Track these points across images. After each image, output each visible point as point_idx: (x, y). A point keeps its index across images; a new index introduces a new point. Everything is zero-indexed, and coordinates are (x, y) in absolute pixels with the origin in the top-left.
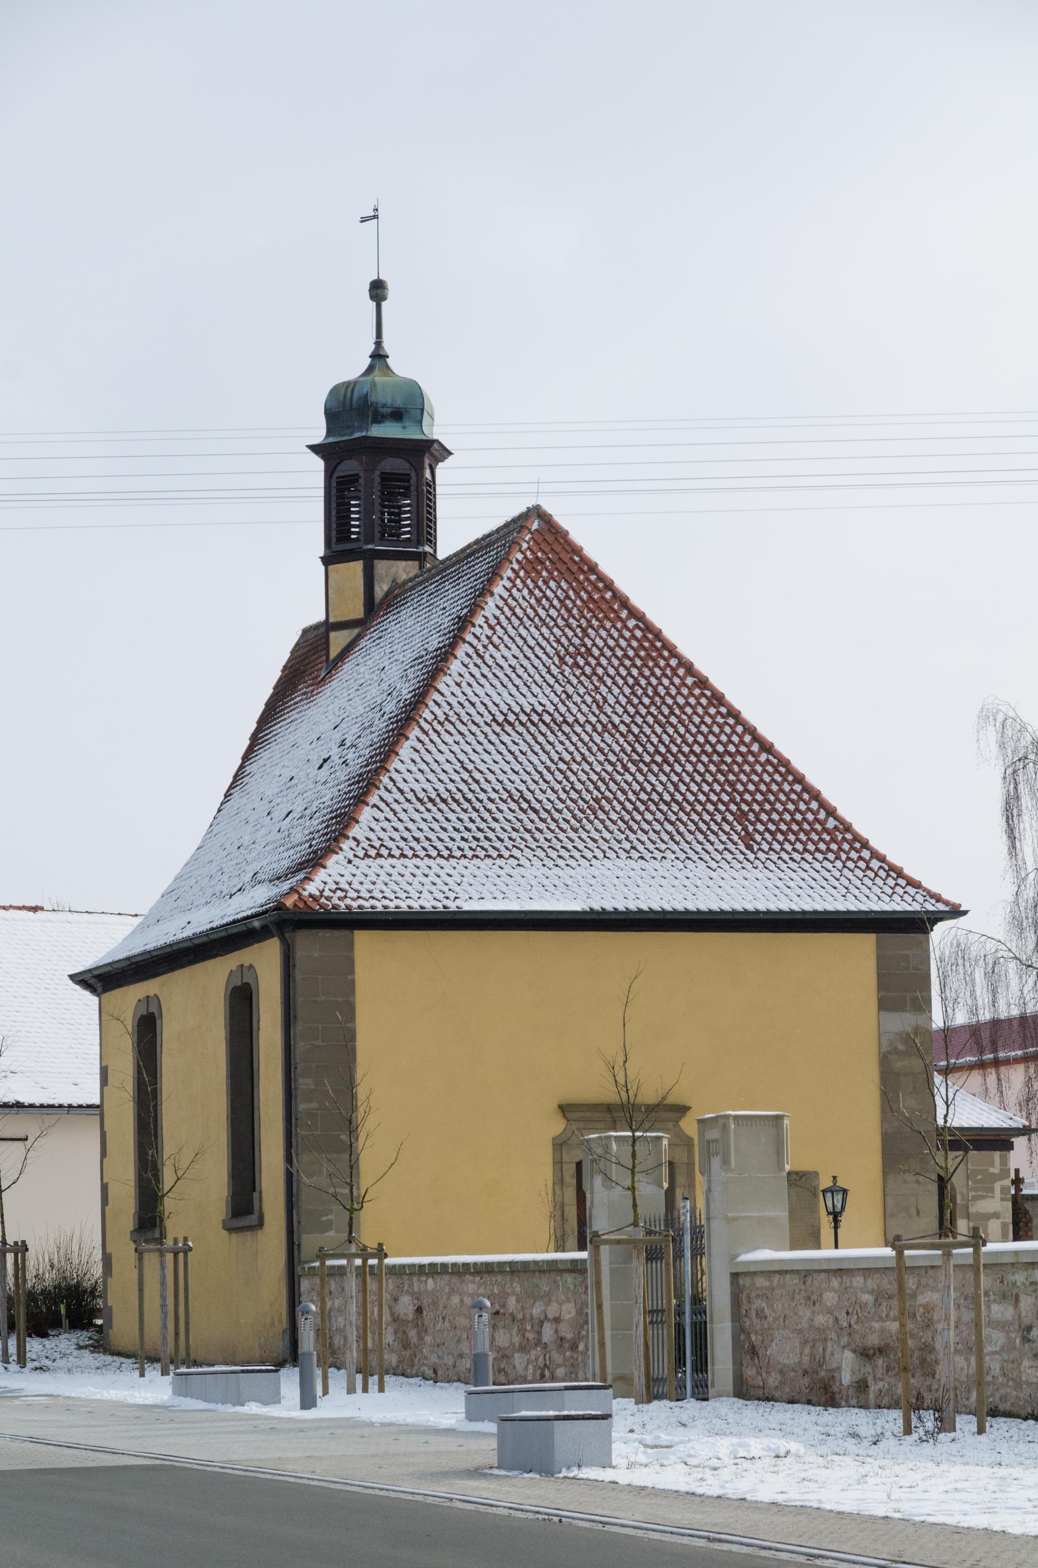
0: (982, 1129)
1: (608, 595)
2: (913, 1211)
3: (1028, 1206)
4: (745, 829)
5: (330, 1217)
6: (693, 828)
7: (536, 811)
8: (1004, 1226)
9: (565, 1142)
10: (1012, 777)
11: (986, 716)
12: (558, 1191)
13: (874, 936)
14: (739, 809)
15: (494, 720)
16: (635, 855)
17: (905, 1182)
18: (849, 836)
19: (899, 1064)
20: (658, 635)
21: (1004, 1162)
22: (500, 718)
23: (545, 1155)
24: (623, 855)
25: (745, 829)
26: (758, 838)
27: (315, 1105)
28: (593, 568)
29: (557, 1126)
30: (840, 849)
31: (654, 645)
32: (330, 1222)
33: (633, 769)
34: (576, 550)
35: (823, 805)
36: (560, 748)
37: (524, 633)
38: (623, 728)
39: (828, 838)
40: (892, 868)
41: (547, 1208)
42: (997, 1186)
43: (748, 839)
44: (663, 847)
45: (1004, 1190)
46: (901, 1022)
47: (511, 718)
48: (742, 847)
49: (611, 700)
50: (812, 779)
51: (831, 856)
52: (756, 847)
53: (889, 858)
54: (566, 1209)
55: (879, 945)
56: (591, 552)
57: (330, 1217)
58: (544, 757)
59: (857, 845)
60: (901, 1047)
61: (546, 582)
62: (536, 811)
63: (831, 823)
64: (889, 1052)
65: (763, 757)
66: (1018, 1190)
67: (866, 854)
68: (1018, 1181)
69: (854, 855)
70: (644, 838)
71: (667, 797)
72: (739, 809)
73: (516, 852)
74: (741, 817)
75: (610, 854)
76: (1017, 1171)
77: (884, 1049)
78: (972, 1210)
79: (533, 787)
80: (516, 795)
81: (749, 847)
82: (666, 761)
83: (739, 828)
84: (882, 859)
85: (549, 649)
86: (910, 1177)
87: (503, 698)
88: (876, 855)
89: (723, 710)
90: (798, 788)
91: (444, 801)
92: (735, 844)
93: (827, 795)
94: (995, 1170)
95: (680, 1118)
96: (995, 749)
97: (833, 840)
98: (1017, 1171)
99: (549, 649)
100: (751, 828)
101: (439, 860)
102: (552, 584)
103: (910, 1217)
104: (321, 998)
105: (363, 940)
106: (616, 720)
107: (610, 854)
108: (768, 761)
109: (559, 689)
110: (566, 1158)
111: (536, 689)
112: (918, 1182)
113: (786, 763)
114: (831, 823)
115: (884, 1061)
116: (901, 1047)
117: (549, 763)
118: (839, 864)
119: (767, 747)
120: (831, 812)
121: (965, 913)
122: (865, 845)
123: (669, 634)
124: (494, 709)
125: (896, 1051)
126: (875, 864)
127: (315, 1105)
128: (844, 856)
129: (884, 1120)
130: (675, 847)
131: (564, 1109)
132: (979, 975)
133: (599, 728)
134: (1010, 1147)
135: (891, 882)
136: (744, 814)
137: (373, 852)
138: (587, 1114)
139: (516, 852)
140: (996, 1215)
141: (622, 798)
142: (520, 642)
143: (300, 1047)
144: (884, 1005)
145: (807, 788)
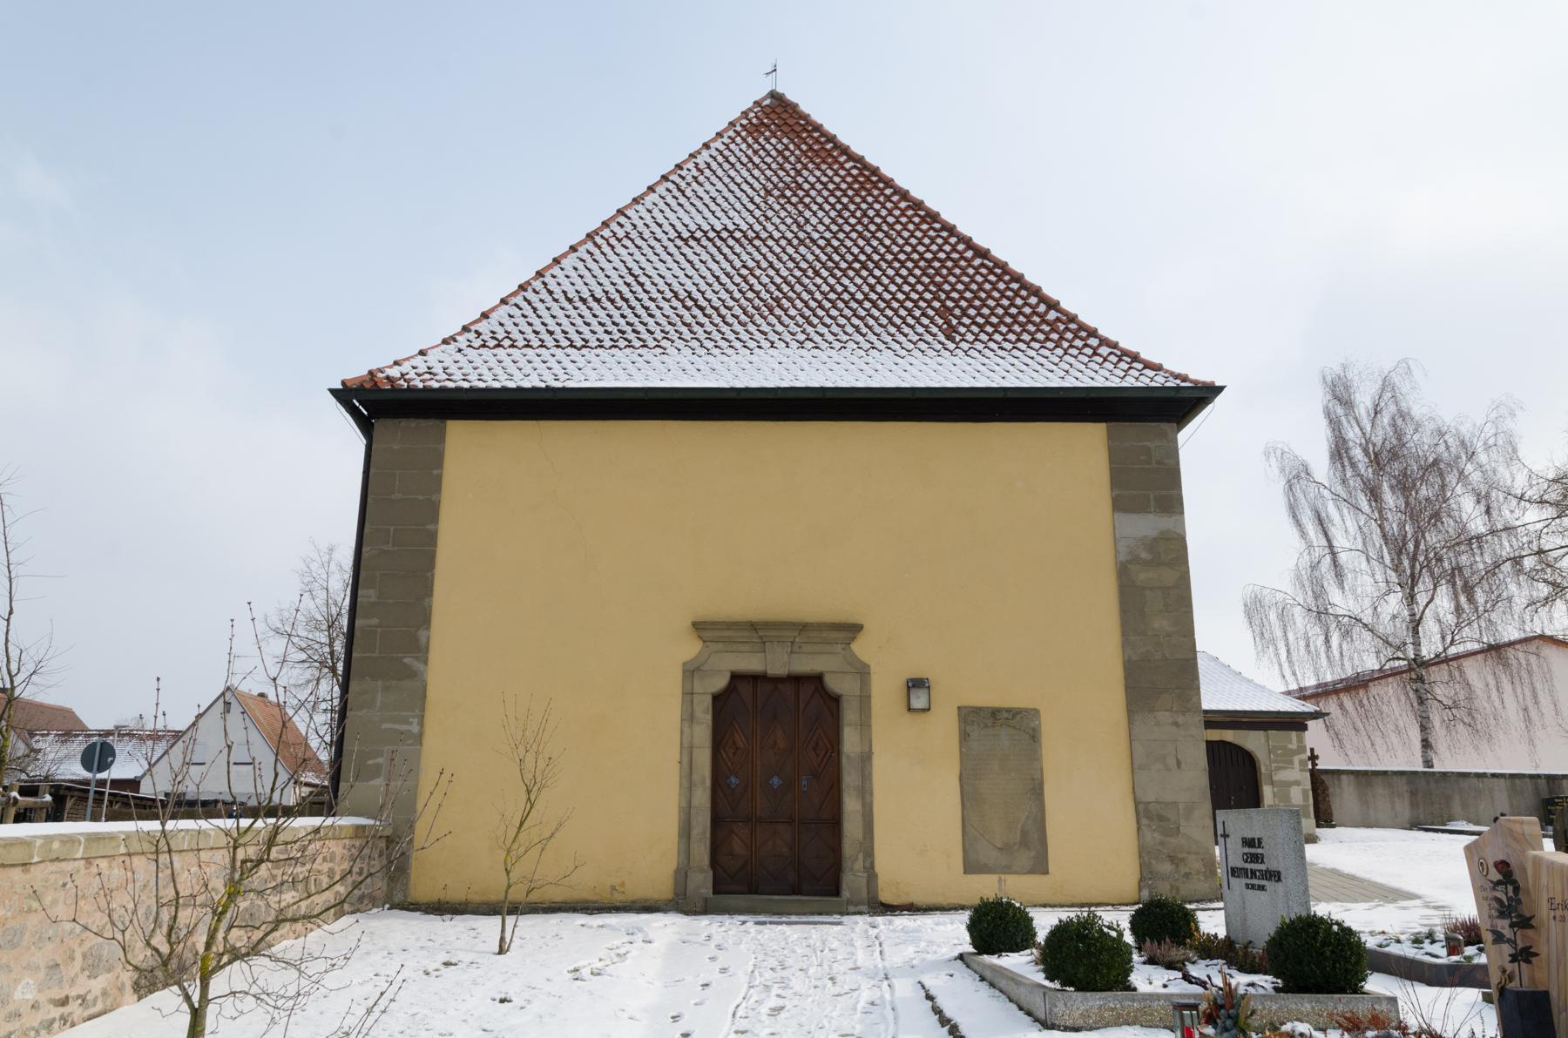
0: (1279, 712)
1: (829, 146)
2: (1172, 762)
3: (1323, 777)
4: (948, 323)
5: (380, 760)
6: (884, 321)
7: (702, 309)
8: (1305, 792)
9: (698, 669)
10: (1290, 486)
11: (1267, 455)
12: (687, 730)
13: (1103, 426)
14: (943, 305)
15: (679, 237)
16: (809, 345)
17: (1158, 724)
18: (1073, 326)
19: (1142, 576)
20: (875, 171)
21: (1301, 740)
22: (686, 235)
23: (673, 685)
24: (794, 345)
25: (948, 323)
26: (962, 330)
27: (375, 621)
28: (818, 128)
29: (691, 648)
30: (1062, 338)
31: (870, 178)
32: (379, 766)
33: (825, 273)
34: (806, 117)
35: (1043, 299)
36: (745, 257)
37: (732, 173)
38: (822, 242)
39: (1047, 328)
40: (1125, 353)
41: (673, 753)
42: (1296, 759)
43: (950, 331)
44: (845, 338)
45: (1302, 763)
46: (1145, 525)
47: (698, 234)
48: (942, 338)
49: (814, 221)
50: (1031, 278)
51: (1050, 345)
52: (958, 338)
53: (1121, 345)
54: (696, 752)
55: (1110, 437)
56: (817, 117)
57: (380, 760)
58: (725, 264)
59: (1084, 334)
60: (1144, 555)
61: (767, 140)
62: (702, 309)
63: (1052, 315)
64: (1129, 562)
65: (977, 262)
66: (1314, 764)
67: (1094, 342)
68: (1313, 758)
69: (1078, 343)
70: (824, 330)
71: (860, 296)
72: (943, 305)
73: (665, 343)
74: (944, 312)
75: (779, 344)
76: (1312, 750)
77: (1122, 558)
78: (1275, 778)
79: (703, 287)
80: (683, 294)
81: (949, 338)
82: (864, 267)
83: (940, 322)
84: (1115, 346)
85: (756, 185)
86: (1164, 716)
87: (693, 219)
88: (1104, 342)
89: (937, 226)
90: (1015, 286)
91: (598, 301)
92: (934, 335)
93: (1048, 291)
94: (1293, 746)
95: (853, 639)
96: (1277, 471)
97: (1054, 330)
98: (1312, 750)
99: (756, 185)
100: (954, 322)
101: (570, 350)
102: (773, 141)
103: (1169, 770)
104: (397, 496)
105: (461, 436)
106: (816, 236)
107: (779, 344)
108: (983, 265)
109: (757, 213)
110: (698, 688)
111: (732, 213)
112: (1176, 724)
113: (1004, 266)
114: (1052, 315)
115: (1123, 572)
116: (1144, 555)
117: (729, 269)
118: (1059, 351)
119: (983, 253)
120: (1053, 305)
121: (1221, 389)
122: (1093, 333)
123: (886, 171)
124: (680, 228)
125: (1136, 560)
126: (1104, 351)
127: (375, 621)
128: (1065, 345)
129: (1126, 643)
130: (860, 339)
131: (699, 627)
132: (1273, 616)
133: (795, 242)
134: (1305, 728)
135: (1124, 366)
136: (950, 310)
137: (492, 343)
138: (727, 633)
139: (665, 343)
140: (1297, 783)
141: (805, 296)
142: (727, 180)
143: (365, 555)
144: (1119, 505)
145: (1025, 285)
